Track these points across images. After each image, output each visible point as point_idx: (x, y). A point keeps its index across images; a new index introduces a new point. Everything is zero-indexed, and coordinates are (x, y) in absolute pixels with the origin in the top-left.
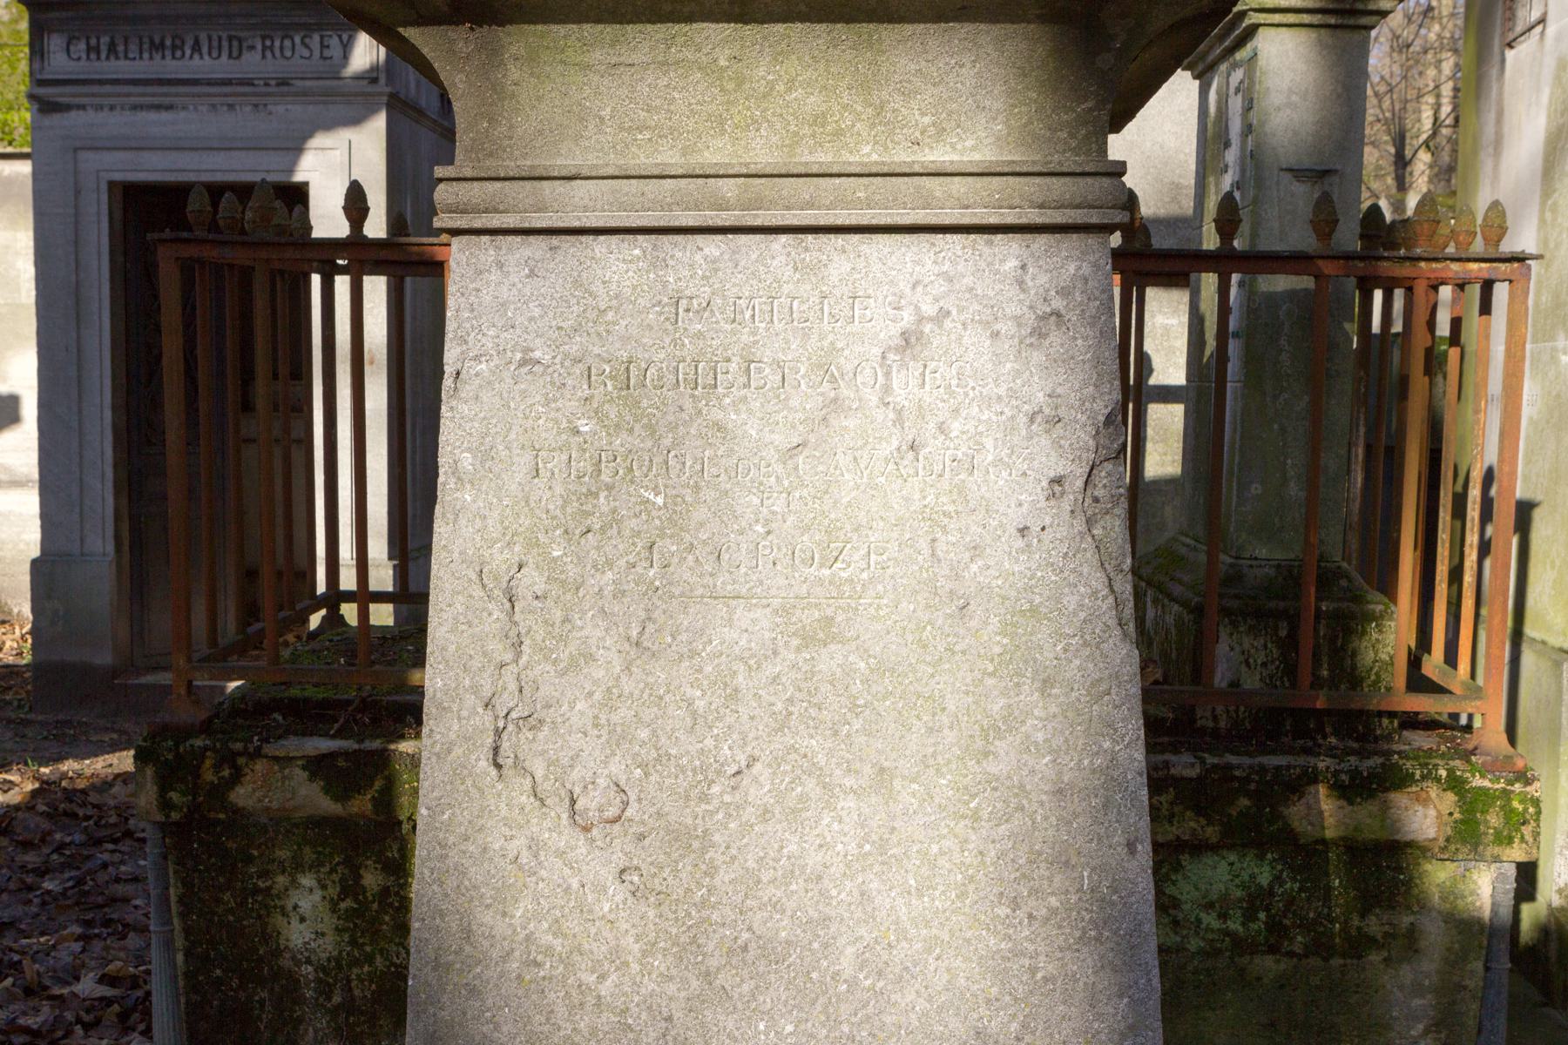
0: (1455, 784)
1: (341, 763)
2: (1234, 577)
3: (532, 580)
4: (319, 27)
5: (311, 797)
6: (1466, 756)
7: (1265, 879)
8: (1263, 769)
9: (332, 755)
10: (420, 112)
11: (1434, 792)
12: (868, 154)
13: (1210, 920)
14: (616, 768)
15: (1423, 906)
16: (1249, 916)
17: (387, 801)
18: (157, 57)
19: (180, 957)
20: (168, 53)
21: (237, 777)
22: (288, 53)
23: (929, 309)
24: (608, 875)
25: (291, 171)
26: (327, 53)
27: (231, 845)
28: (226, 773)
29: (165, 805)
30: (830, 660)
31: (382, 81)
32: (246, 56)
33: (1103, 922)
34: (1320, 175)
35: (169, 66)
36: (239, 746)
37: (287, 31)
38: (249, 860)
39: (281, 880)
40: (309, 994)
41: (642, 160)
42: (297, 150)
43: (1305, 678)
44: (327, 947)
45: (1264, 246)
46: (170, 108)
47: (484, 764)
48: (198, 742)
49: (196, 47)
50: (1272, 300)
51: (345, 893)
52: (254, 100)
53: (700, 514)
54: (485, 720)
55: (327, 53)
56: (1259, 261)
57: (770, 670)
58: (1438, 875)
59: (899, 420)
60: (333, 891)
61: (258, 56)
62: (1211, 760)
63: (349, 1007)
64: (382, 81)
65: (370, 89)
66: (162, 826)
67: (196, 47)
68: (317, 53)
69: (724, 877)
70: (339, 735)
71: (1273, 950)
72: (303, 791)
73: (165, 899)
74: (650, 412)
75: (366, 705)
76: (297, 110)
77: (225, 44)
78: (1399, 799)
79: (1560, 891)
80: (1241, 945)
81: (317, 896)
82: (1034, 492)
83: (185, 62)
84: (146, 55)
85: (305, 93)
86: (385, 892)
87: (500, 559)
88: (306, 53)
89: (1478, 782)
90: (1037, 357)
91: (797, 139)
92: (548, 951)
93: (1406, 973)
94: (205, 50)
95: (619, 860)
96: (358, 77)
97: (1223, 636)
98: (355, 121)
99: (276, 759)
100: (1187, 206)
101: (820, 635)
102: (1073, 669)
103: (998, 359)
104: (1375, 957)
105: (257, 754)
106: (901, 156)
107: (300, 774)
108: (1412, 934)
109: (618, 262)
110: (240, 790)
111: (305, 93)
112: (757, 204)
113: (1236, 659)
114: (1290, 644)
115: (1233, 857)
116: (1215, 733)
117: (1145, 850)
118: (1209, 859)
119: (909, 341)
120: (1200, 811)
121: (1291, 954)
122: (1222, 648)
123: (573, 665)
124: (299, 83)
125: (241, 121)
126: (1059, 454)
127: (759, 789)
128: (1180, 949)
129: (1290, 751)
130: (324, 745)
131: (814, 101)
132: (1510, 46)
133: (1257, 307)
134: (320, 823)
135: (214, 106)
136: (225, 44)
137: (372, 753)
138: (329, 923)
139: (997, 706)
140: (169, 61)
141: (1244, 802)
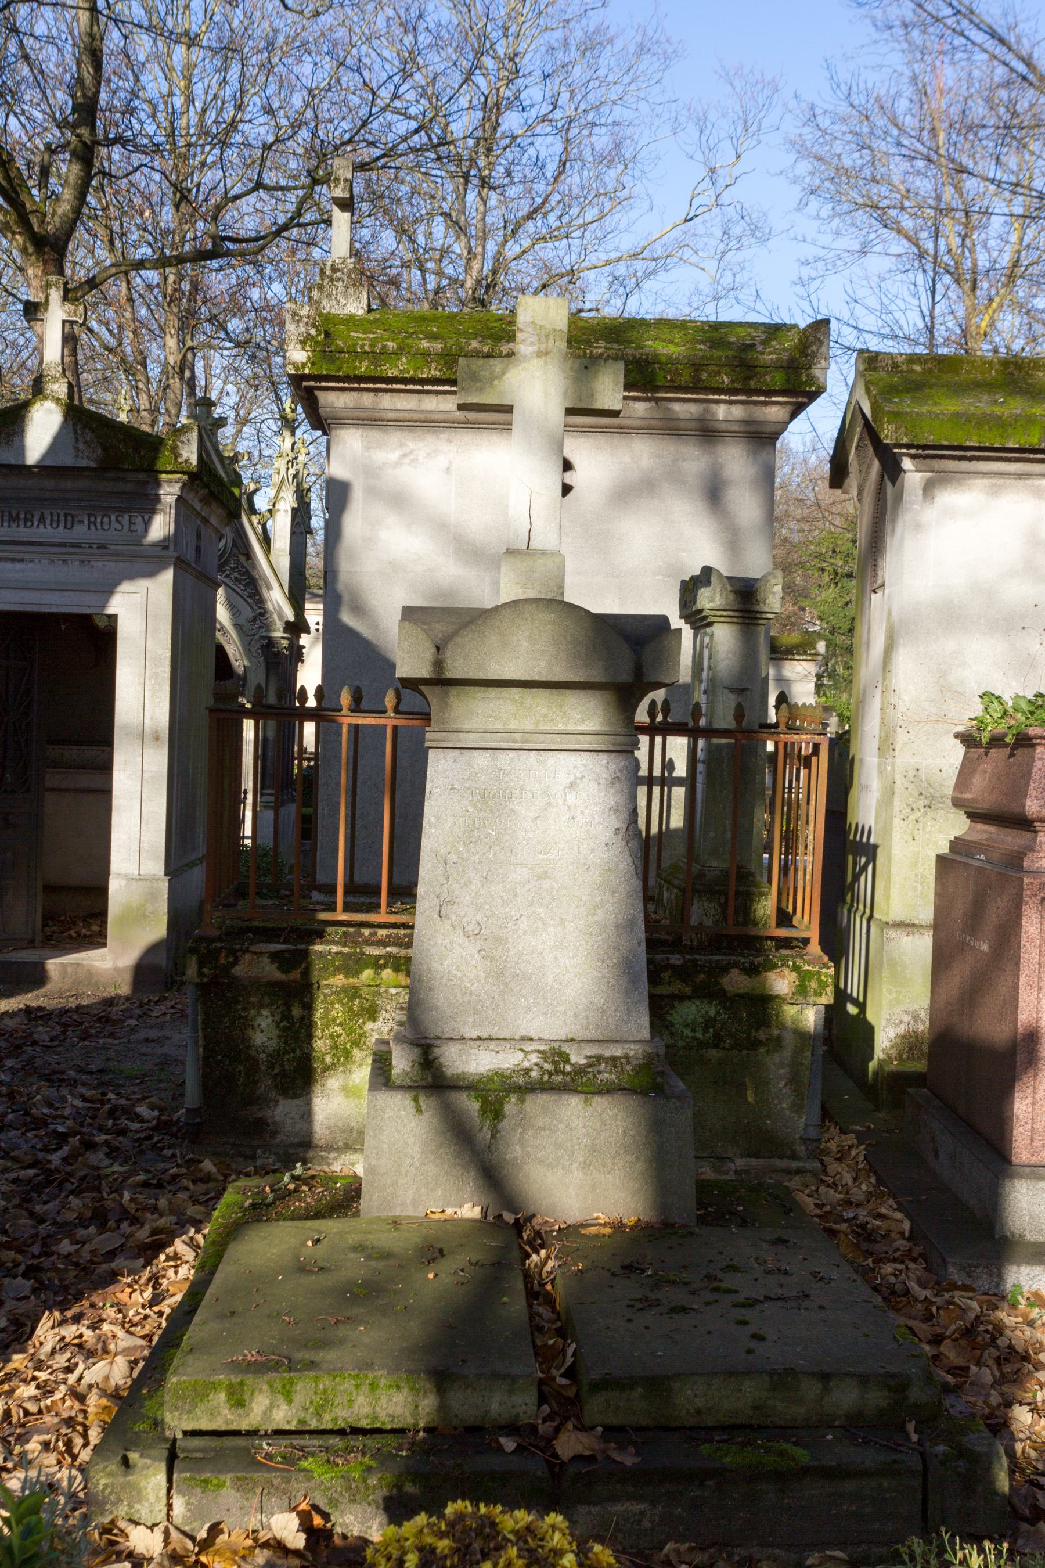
0: (796, 968)
1: (287, 955)
2: (701, 876)
3: (453, 857)
4: (129, 510)
5: (271, 971)
6: (801, 957)
7: (712, 1013)
8: (710, 962)
9: (282, 951)
10: (188, 564)
11: (787, 972)
12: (561, 727)
13: (688, 1032)
14: (478, 917)
15: (782, 1026)
16: (705, 1030)
17: (306, 973)
18: (14, 525)
19: (201, 1050)
20: (21, 523)
21: (236, 962)
22: (106, 527)
23: (579, 775)
24: (475, 951)
25: (104, 607)
26: (133, 528)
27: (230, 995)
28: (231, 959)
29: (201, 974)
30: (546, 884)
31: (172, 548)
32: (77, 528)
33: (627, 968)
34: (741, 691)
35: (21, 532)
36: (238, 947)
37: (106, 511)
38: (237, 1002)
39: (253, 1012)
40: (263, 1068)
41: (491, 727)
42: (109, 591)
43: (731, 921)
44: (273, 1045)
45: (715, 726)
46: (21, 560)
47: (436, 916)
48: (218, 945)
49: (42, 520)
50: (719, 746)
51: (284, 1018)
52: (81, 558)
53: (507, 838)
54: (436, 902)
55: (133, 528)
56: (709, 732)
57: (527, 887)
58: (790, 1011)
59: (569, 809)
60: (278, 1018)
61: (85, 528)
62: (688, 957)
63: (283, 1074)
64: (172, 548)
65: (164, 553)
66: (197, 985)
67: (42, 520)
68: (126, 527)
69: (512, 952)
70: (284, 942)
71: (716, 1046)
72: (267, 969)
73: (195, 1021)
74: (493, 803)
75: (293, 930)
76: (111, 565)
77: (62, 518)
78: (772, 975)
79: (883, 1051)
80: (701, 1044)
81: (270, 1020)
82: (610, 833)
83: (34, 530)
84: (6, 524)
85: (117, 554)
86: (303, 1018)
87: (443, 851)
88: (119, 527)
89: (806, 968)
90: (612, 791)
91: (539, 721)
92: (455, 976)
93: (776, 1058)
94: (48, 522)
95: (479, 947)
96: (154, 545)
97: (695, 902)
98: (151, 574)
99: (255, 953)
101: (544, 876)
102: (621, 889)
103: (599, 791)
104: (762, 1050)
105: (247, 951)
106: (571, 728)
107: (266, 960)
108: (779, 1039)
109: (482, 759)
110: (237, 968)
111: (117, 554)
112: (527, 741)
113: (701, 913)
114: (724, 907)
115: (698, 1003)
116: (692, 948)
117: (643, 944)
118: (687, 1003)
119: (572, 785)
120: (683, 981)
121: (724, 1048)
122: (695, 908)
123: (465, 885)
124: (113, 547)
125: (73, 572)
126: (616, 822)
127: (524, 924)
128: (674, 1046)
129: (724, 954)
130: (279, 947)
131: (544, 710)
132: (875, 592)
133: (710, 750)
134: (273, 984)
135: (53, 561)
136: (62, 518)
137: (301, 951)
138: (275, 1033)
139: (598, 899)
140: (22, 529)
141: (703, 976)
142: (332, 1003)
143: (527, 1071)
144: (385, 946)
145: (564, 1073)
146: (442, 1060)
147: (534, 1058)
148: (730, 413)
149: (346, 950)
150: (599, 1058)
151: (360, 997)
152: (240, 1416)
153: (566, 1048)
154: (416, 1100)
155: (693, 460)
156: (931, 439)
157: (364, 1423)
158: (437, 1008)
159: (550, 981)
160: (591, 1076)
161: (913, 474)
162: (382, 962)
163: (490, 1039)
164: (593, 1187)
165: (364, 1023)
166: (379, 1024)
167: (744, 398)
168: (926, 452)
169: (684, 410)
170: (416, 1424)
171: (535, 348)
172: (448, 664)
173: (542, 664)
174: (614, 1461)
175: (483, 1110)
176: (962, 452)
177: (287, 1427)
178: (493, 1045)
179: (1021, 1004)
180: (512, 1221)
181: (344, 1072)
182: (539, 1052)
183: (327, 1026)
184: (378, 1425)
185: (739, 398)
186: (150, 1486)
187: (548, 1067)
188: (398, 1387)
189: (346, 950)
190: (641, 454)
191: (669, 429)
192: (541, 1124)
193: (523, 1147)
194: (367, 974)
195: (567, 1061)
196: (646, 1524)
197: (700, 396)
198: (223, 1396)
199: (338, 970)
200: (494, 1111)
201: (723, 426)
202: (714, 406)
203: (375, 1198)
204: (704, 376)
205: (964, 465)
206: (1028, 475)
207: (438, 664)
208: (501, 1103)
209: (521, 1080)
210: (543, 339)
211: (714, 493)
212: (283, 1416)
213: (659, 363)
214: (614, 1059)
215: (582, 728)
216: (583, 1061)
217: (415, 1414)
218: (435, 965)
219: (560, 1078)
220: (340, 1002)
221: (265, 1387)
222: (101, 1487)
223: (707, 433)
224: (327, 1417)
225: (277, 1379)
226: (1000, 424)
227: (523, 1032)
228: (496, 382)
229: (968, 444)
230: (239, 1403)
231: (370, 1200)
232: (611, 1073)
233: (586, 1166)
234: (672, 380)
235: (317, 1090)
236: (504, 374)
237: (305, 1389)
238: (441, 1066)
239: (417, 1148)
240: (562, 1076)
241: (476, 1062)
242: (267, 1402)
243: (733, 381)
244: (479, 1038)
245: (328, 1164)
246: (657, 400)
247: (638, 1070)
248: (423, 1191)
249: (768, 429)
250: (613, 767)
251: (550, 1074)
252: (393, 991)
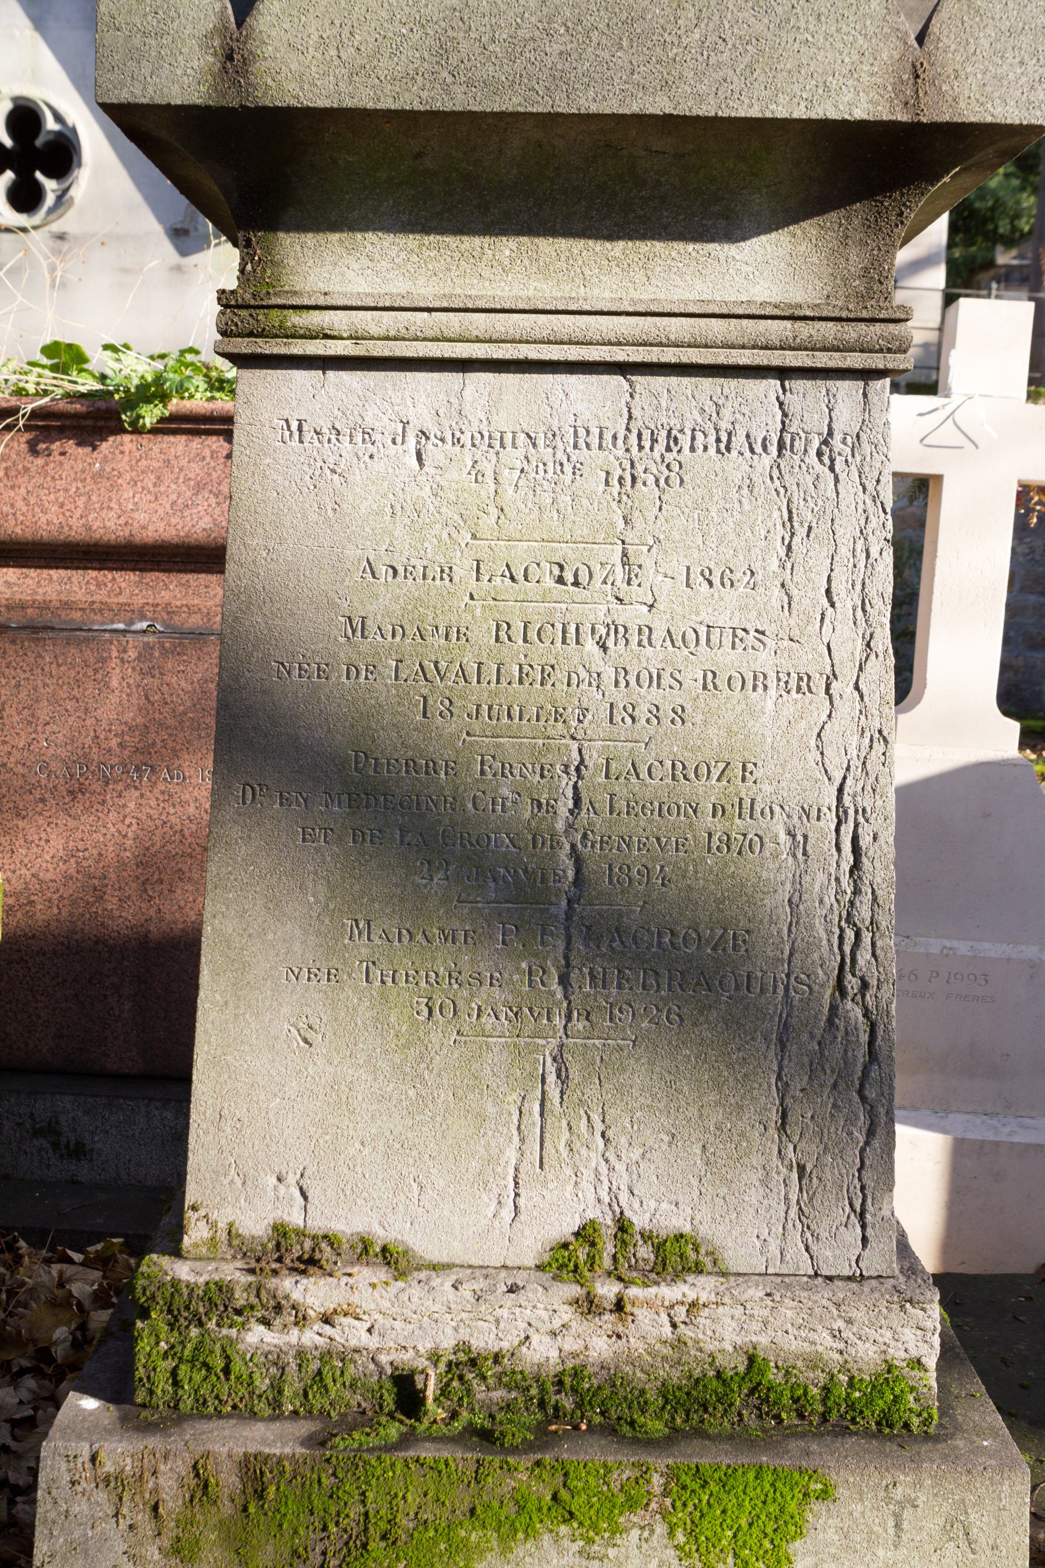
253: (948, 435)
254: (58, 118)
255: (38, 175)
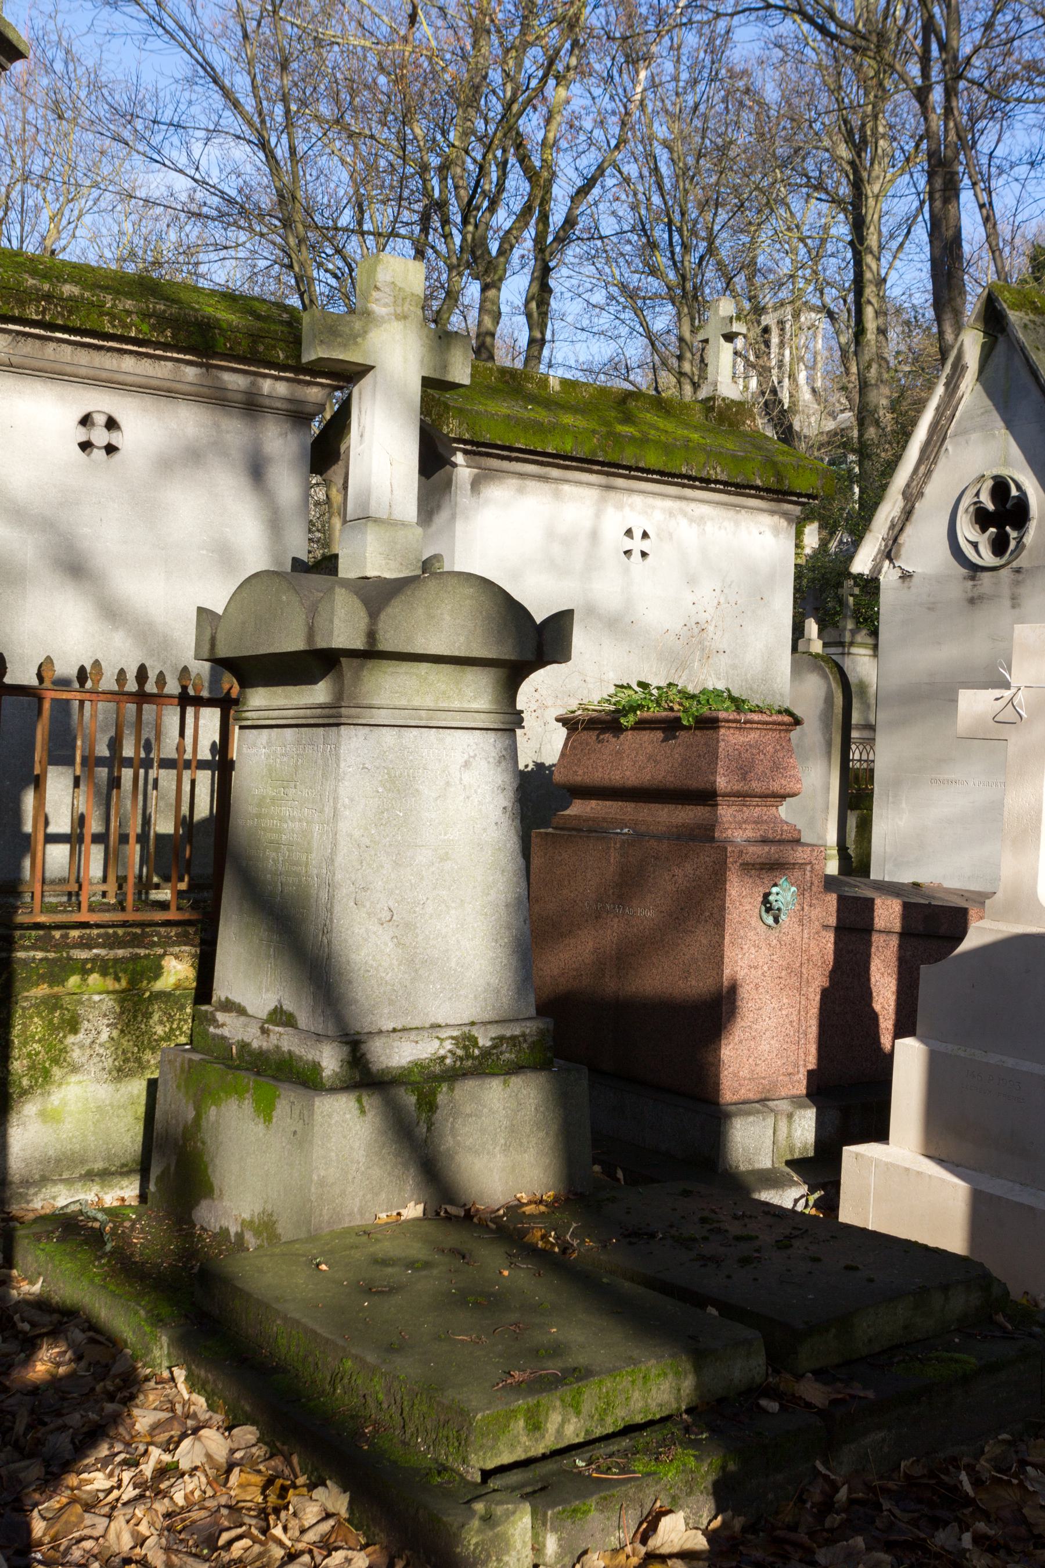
12: (456, 705)
14: (391, 904)
47: (352, 904)
69: (420, 938)
91: (438, 698)
95: (391, 934)
100: (66, 875)
106: (466, 706)
109: (389, 736)
112: (431, 719)
119: (467, 765)
142: (32, 1017)
143: (443, 1058)
144: (90, 948)
145: (474, 1058)
146: (368, 1056)
147: (448, 1045)
148: (274, 389)
149: (51, 955)
150: (501, 1039)
151: (61, 1007)
152: (537, 1440)
153: (475, 1032)
154: (359, 1100)
155: (234, 430)
156: (488, 437)
157: (639, 1419)
158: (356, 1001)
159: (453, 965)
160: (494, 1057)
161: (463, 468)
162: (89, 966)
163: (404, 1030)
164: (513, 1168)
165: (65, 1037)
166: (81, 1036)
167: (291, 375)
168: (479, 449)
169: (235, 381)
170: (678, 1409)
171: (391, 309)
172: (380, 636)
173: (462, 639)
174: (860, 1398)
175: (419, 1103)
176: (509, 452)
177: (577, 1441)
178: (413, 1035)
179: (726, 960)
180: (462, 1214)
181: (42, 1094)
182: (452, 1038)
183: (25, 1044)
184: (650, 1417)
185: (287, 375)
186: (517, 1532)
187: (460, 1052)
188: (665, 1374)
189: (51, 955)
190: (188, 421)
191: (216, 399)
192: (468, 1111)
193: (454, 1137)
194: (74, 980)
195: (475, 1044)
196: (886, 1450)
197: (252, 368)
198: (521, 1423)
199: (42, 978)
200: (428, 1104)
201: (267, 402)
202: (260, 380)
203: (325, 1211)
204: (261, 348)
205: (505, 465)
206: (557, 480)
207: (371, 636)
208: (433, 1093)
209: (437, 1069)
210: (400, 301)
211: (256, 470)
212: (573, 1431)
213: (220, 328)
214: (513, 1038)
215: (475, 706)
216: (489, 1044)
217: (678, 1399)
218: (353, 956)
219: (470, 1063)
220: (39, 1015)
221: (558, 1403)
222: (472, 1547)
223: (251, 406)
224: (609, 1420)
225: (566, 1392)
226: (539, 428)
227: (433, 1020)
228: (359, 340)
229: (517, 445)
230: (535, 1427)
231: (321, 1215)
232: (511, 1052)
233: (506, 1148)
234: (231, 349)
235: (14, 1119)
236: (366, 332)
237: (591, 1395)
238: (367, 1062)
239: (362, 1152)
240: (474, 1063)
241: (399, 1054)
242: (560, 1419)
243: (287, 357)
244: (394, 1030)
245: (28, 1202)
246: (208, 367)
247: (533, 1046)
248: (369, 1196)
249: (310, 409)
250: (499, 745)
251: (461, 1059)
252: (96, 998)
253: (1009, 715)
254: (1019, 487)
255: (1008, 528)
